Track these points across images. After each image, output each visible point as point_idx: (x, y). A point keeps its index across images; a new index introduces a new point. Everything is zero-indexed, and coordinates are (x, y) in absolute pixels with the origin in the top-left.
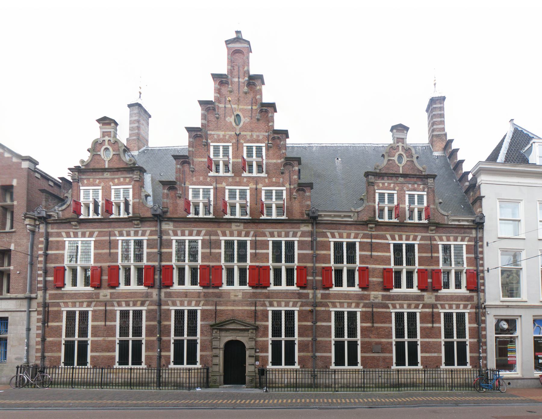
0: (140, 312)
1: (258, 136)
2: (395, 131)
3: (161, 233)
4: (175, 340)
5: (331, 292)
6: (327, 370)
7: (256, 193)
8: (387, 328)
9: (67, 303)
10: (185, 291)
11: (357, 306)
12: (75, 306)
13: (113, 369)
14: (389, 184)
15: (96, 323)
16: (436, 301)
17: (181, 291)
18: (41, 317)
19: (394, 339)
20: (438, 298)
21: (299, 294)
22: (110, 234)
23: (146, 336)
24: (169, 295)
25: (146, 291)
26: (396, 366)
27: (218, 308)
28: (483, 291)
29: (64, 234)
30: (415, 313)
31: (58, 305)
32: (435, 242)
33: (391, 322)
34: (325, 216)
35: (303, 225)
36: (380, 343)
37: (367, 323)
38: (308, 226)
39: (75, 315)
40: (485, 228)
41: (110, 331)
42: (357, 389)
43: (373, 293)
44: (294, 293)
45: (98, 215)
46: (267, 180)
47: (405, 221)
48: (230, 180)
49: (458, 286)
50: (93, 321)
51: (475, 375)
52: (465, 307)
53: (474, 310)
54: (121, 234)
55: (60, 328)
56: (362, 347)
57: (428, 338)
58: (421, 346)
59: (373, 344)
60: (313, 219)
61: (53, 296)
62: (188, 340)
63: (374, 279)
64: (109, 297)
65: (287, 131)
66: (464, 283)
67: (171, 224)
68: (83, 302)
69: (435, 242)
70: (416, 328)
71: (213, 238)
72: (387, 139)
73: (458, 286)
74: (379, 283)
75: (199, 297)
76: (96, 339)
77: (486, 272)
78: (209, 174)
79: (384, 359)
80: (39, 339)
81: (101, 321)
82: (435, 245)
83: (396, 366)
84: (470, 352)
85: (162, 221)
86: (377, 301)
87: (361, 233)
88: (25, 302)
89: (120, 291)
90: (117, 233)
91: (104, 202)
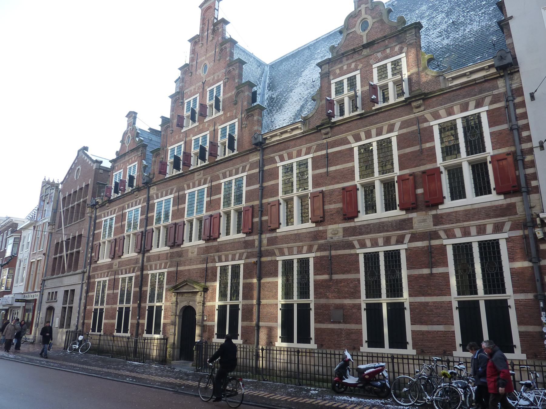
0: (307, 260)
4: (367, 304)
5: (278, 235)
8: (352, 280)
10: (158, 253)
11: (310, 251)
13: (273, 350)
14: (349, 65)
16: (434, 225)
19: (363, 300)
20: (438, 220)
25: (204, 246)
26: (369, 346)
27: (180, 268)
28: (537, 190)
30: (398, 251)
32: (425, 125)
33: (358, 271)
34: (272, 137)
35: (252, 155)
36: (341, 307)
37: (323, 274)
40: (521, 70)
42: (321, 384)
45: (118, 194)
52: (498, 228)
56: (316, 314)
57: (424, 295)
59: (332, 308)
60: (260, 145)
62: (230, 305)
63: (332, 206)
69: (425, 125)
74: (338, 211)
77: (537, 151)
78: (182, 131)
79: (349, 332)
82: (425, 129)
83: (369, 346)
84: (520, 323)
85: (151, 187)
86: (336, 238)
87: (314, 145)
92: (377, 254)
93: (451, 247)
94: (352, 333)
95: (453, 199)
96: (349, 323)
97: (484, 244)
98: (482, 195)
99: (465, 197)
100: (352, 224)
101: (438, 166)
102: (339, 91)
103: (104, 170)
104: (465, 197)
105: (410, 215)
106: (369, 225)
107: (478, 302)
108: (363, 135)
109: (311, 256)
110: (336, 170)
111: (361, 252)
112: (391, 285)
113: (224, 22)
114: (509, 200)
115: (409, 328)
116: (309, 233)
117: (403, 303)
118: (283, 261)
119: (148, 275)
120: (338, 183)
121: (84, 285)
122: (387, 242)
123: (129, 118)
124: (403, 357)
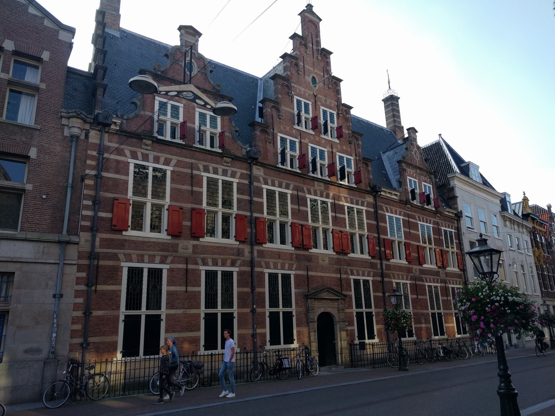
1: (331, 103)
3: (250, 178)
4: (205, 314)
5: (391, 264)
7: (332, 155)
9: (130, 255)
12: (143, 261)
15: (173, 288)
17: (275, 250)
18: (84, 275)
19: (203, 310)
21: (371, 263)
22: (192, 167)
23: (239, 307)
24: (262, 254)
25: (237, 246)
29: (128, 153)
30: (161, 270)
31: (115, 257)
38: (259, 169)
39: (217, 276)
41: (192, 300)
44: (366, 262)
46: (339, 146)
47: (194, 145)
48: (312, 138)
49: (155, 228)
50: (169, 284)
54: (206, 170)
55: (117, 294)
61: (107, 243)
62: (222, 314)
64: (190, 250)
66: (233, 232)
67: (262, 169)
68: (154, 256)
70: (233, 294)
71: (300, 194)
72: (173, 39)
73: (226, 234)
75: (291, 260)
76: (173, 312)
80: (79, 314)
81: (180, 285)
88: (55, 250)
89: (206, 244)
90: (201, 167)
93: (127, 269)
97: (133, 270)
100: (118, 237)
101: (129, 198)
107: (217, 314)
109: (235, 270)
111: (203, 269)
112: (214, 300)
114: (241, 246)
117: (292, 312)
123: (284, 62)
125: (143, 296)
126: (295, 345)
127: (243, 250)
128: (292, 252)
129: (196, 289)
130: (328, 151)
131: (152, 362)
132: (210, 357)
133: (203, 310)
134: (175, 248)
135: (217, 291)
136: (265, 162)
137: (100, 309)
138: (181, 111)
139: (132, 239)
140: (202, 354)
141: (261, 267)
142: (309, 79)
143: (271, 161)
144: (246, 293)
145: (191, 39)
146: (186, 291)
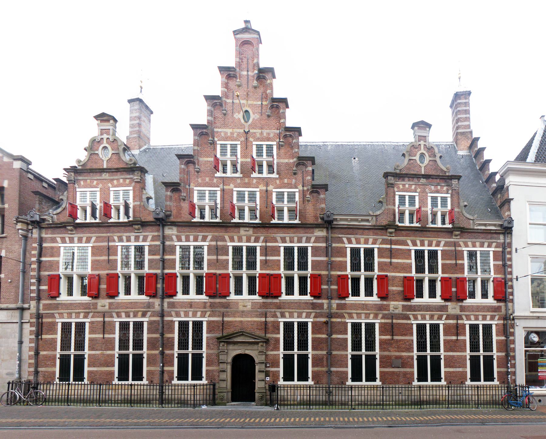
2: (416, 128)
5: (347, 302)
6: (464, 386)
7: (267, 195)
12: (71, 317)
14: (410, 185)
17: (186, 301)
19: (415, 353)
20: (462, 309)
21: (313, 304)
22: (455, 244)
23: (148, 349)
24: (172, 305)
25: (147, 301)
27: (226, 319)
28: (512, 301)
29: (59, 240)
32: (459, 249)
34: (341, 220)
35: (317, 230)
37: (386, 335)
40: (513, 233)
41: (109, 344)
43: (392, 303)
45: (95, 220)
46: (278, 182)
47: (427, 226)
48: (239, 181)
51: (503, 391)
52: (492, 318)
53: (502, 322)
54: (121, 240)
55: (54, 341)
56: (380, 362)
58: (444, 360)
60: (328, 223)
61: (47, 307)
63: (394, 288)
64: (107, 307)
65: (300, 128)
66: (491, 293)
68: (79, 313)
69: (459, 249)
71: (220, 243)
72: (407, 137)
74: (399, 292)
75: (205, 307)
77: (514, 281)
79: (405, 374)
81: (99, 333)
82: (459, 251)
84: (498, 367)
86: (397, 311)
87: (380, 238)
90: (116, 238)
91: (102, 205)
92: (187, 322)
94: (407, 374)
95: (192, 380)
96: (405, 368)
98: (289, 295)
99: (359, 296)
100: (409, 303)
102: (224, 153)
103: (35, 176)
104: (359, 296)
105: (447, 304)
106: (420, 305)
107: (294, 355)
108: (304, 239)
110: (398, 263)
111: (349, 321)
113: (297, 131)
114: (152, 300)
115: (443, 370)
116: (375, 305)
118: (417, 324)
119: (173, 322)
120: (399, 272)
121: (27, 328)
122: (432, 317)
124: (439, 386)
125: (203, 343)
126: (204, 381)
127: (154, 303)
128: (205, 301)
129: (111, 336)
130: (261, 191)
131: (77, 386)
132: (130, 387)
133: (58, 352)
134: (386, 308)
135: (426, 339)
136: (179, 220)
137: (45, 351)
138: (417, 199)
139: (63, 302)
140: (117, 383)
141: (171, 316)
142: (239, 116)
143: (185, 217)
144: (156, 338)
145: (422, 133)
146: (104, 338)
